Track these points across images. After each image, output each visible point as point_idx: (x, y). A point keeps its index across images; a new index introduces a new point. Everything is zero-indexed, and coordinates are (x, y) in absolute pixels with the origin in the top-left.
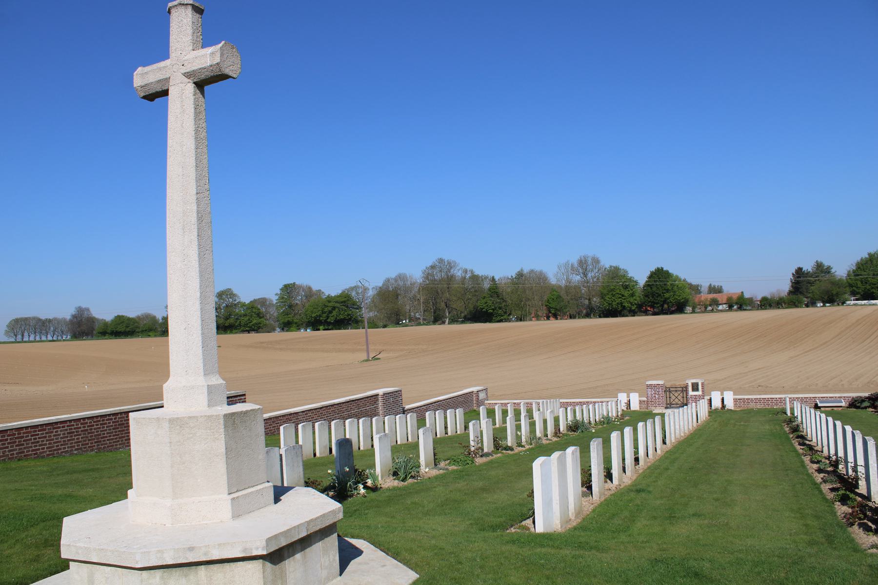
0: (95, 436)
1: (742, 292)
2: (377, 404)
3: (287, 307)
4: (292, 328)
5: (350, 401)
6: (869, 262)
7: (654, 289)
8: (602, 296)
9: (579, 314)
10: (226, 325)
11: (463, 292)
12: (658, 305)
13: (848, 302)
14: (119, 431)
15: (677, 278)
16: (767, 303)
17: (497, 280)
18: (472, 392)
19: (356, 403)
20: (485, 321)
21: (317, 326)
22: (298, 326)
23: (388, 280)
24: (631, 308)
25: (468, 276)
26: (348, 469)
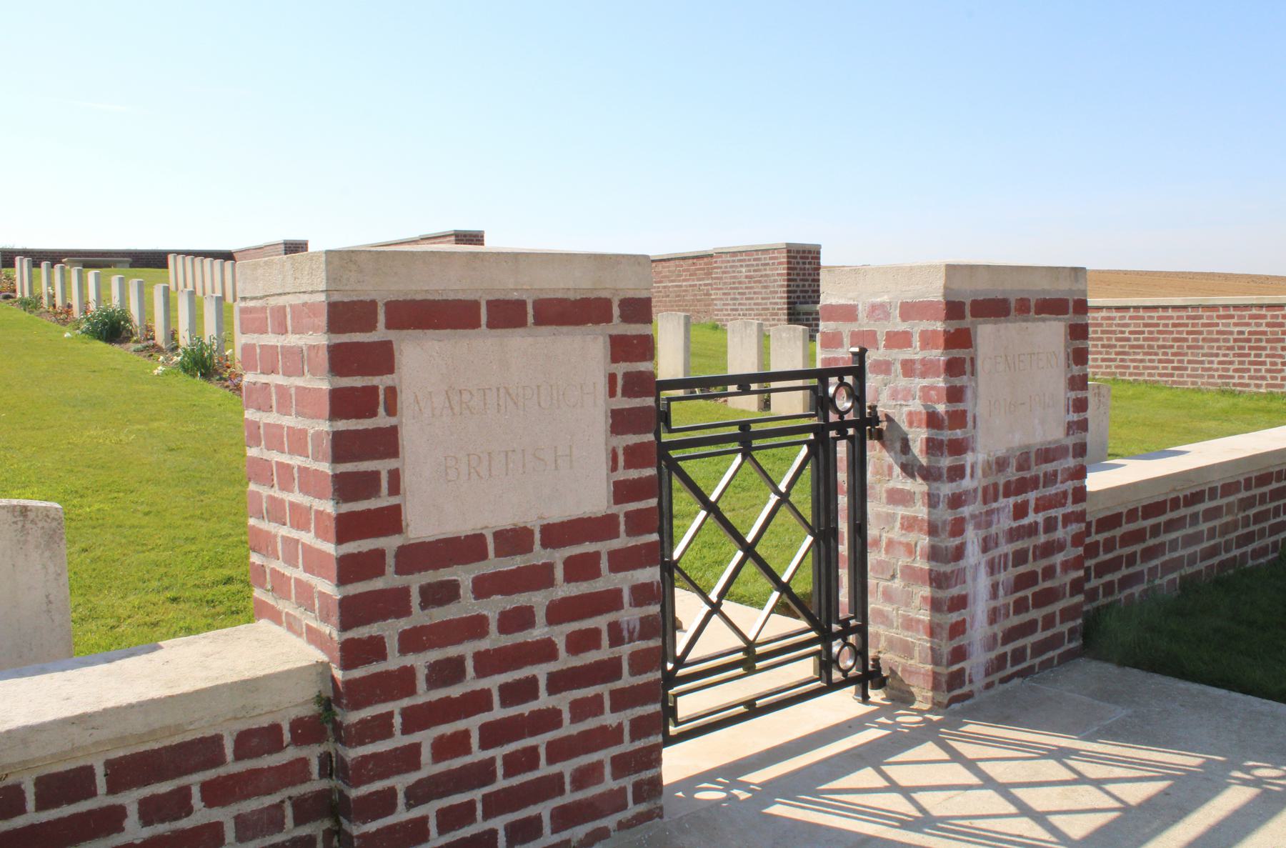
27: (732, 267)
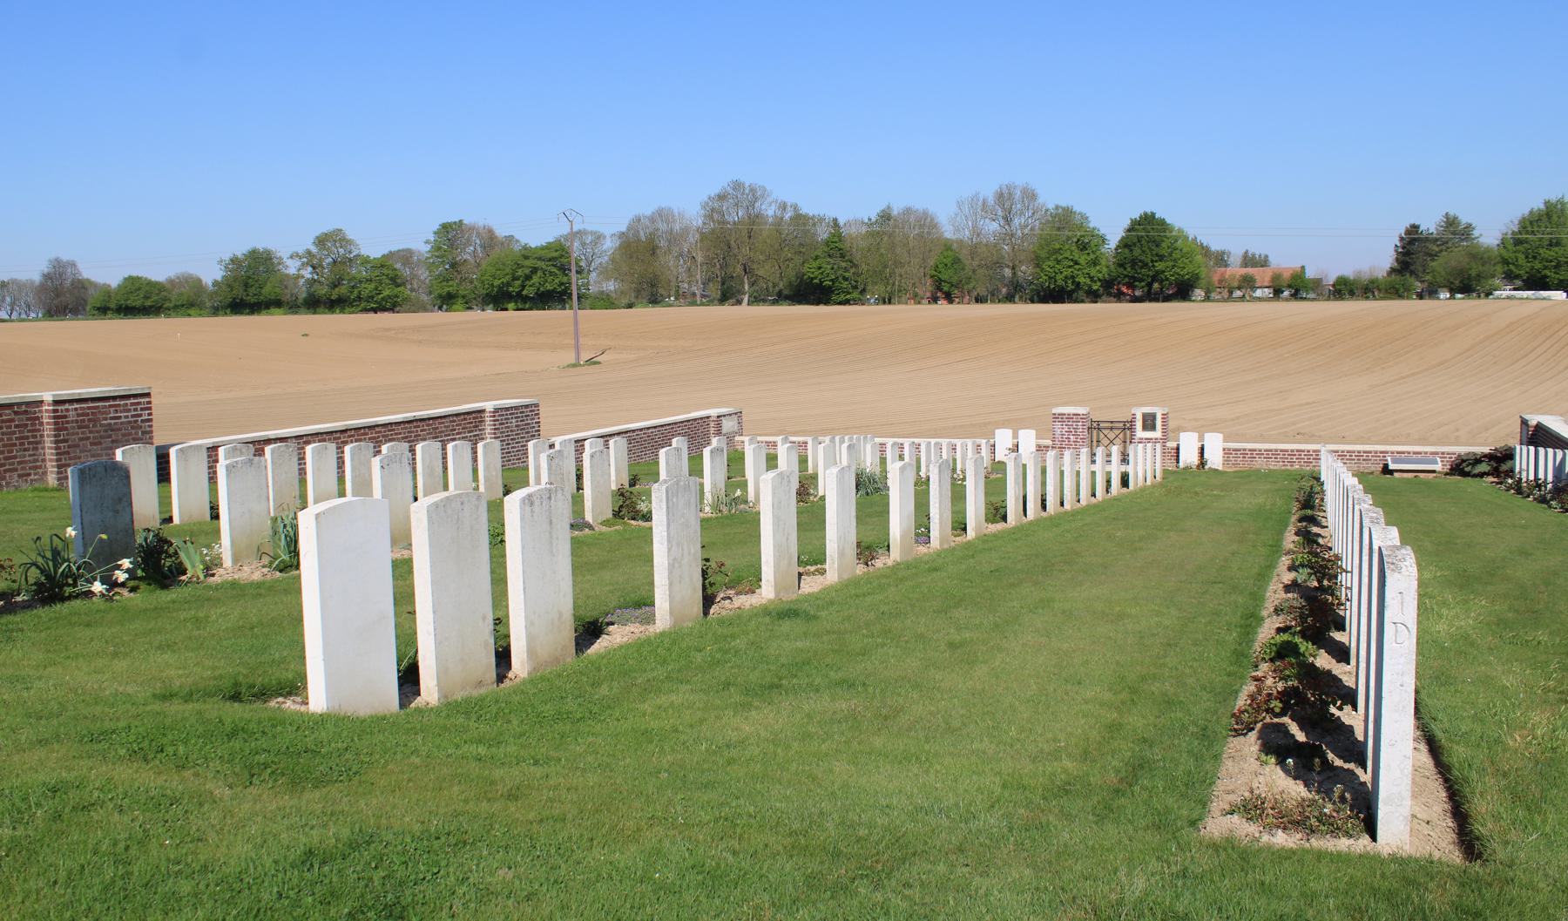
1: (1303, 267)
2: (480, 430)
3: (447, 267)
4: (454, 307)
5: (416, 420)
6: (1545, 218)
7: (1137, 252)
8: (1037, 262)
9: (993, 295)
10: (332, 298)
11: (777, 246)
12: (1143, 284)
13: (1497, 293)
15: (1182, 235)
16: (1344, 289)
17: (841, 224)
18: (708, 417)
19: (431, 425)
21: (503, 305)
22: (466, 303)
24: (1090, 287)
25: (787, 216)
26: (73, 533)
27: (506, 419)
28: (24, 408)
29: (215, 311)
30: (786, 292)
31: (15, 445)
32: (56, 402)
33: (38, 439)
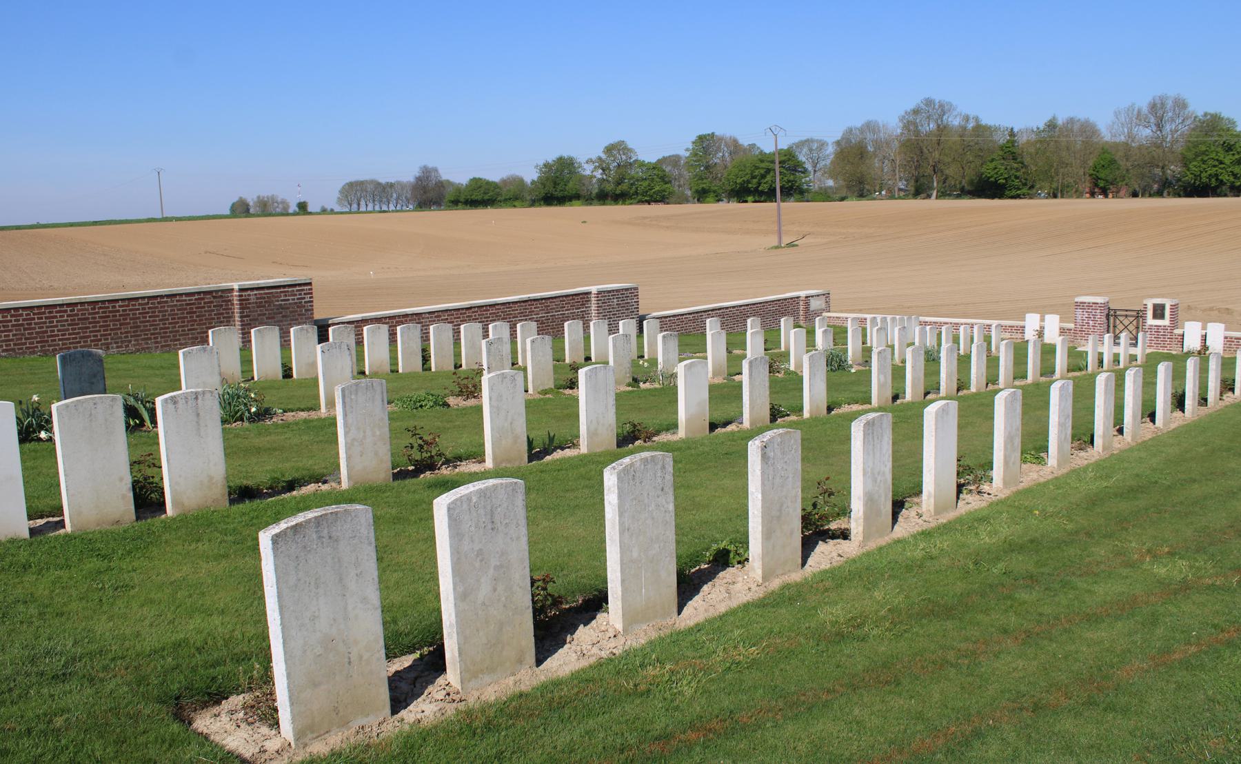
0: (37, 333)
3: (702, 169)
4: (708, 199)
5: (531, 300)
8: (1185, 162)
11: (960, 151)
14: (79, 329)
18: (798, 298)
20: (992, 197)
22: (717, 196)
23: (850, 131)
28: (220, 293)
29: (533, 203)
30: (967, 188)
31: (214, 319)
32: (241, 290)
33: (231, 314)
